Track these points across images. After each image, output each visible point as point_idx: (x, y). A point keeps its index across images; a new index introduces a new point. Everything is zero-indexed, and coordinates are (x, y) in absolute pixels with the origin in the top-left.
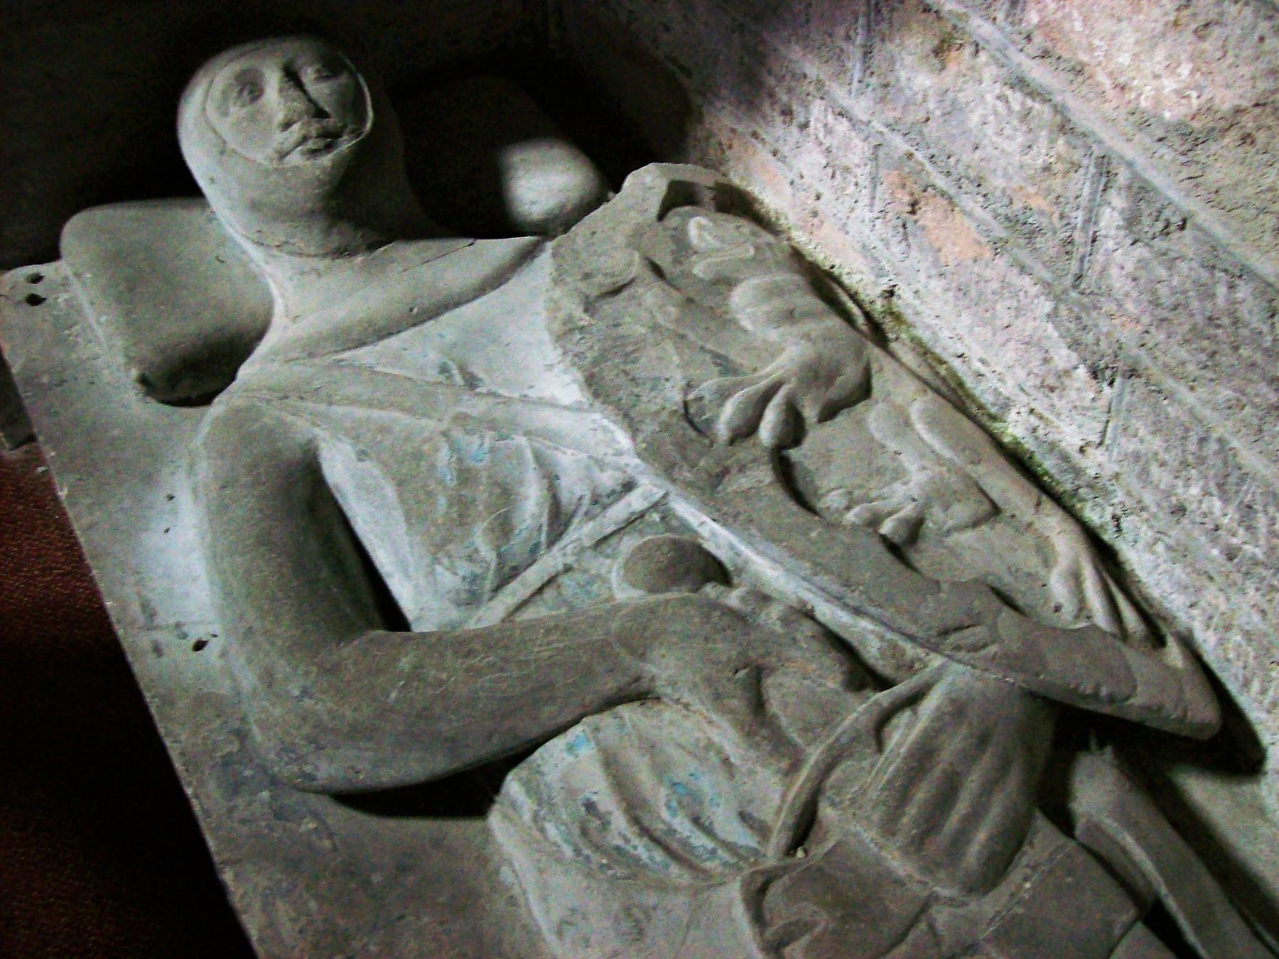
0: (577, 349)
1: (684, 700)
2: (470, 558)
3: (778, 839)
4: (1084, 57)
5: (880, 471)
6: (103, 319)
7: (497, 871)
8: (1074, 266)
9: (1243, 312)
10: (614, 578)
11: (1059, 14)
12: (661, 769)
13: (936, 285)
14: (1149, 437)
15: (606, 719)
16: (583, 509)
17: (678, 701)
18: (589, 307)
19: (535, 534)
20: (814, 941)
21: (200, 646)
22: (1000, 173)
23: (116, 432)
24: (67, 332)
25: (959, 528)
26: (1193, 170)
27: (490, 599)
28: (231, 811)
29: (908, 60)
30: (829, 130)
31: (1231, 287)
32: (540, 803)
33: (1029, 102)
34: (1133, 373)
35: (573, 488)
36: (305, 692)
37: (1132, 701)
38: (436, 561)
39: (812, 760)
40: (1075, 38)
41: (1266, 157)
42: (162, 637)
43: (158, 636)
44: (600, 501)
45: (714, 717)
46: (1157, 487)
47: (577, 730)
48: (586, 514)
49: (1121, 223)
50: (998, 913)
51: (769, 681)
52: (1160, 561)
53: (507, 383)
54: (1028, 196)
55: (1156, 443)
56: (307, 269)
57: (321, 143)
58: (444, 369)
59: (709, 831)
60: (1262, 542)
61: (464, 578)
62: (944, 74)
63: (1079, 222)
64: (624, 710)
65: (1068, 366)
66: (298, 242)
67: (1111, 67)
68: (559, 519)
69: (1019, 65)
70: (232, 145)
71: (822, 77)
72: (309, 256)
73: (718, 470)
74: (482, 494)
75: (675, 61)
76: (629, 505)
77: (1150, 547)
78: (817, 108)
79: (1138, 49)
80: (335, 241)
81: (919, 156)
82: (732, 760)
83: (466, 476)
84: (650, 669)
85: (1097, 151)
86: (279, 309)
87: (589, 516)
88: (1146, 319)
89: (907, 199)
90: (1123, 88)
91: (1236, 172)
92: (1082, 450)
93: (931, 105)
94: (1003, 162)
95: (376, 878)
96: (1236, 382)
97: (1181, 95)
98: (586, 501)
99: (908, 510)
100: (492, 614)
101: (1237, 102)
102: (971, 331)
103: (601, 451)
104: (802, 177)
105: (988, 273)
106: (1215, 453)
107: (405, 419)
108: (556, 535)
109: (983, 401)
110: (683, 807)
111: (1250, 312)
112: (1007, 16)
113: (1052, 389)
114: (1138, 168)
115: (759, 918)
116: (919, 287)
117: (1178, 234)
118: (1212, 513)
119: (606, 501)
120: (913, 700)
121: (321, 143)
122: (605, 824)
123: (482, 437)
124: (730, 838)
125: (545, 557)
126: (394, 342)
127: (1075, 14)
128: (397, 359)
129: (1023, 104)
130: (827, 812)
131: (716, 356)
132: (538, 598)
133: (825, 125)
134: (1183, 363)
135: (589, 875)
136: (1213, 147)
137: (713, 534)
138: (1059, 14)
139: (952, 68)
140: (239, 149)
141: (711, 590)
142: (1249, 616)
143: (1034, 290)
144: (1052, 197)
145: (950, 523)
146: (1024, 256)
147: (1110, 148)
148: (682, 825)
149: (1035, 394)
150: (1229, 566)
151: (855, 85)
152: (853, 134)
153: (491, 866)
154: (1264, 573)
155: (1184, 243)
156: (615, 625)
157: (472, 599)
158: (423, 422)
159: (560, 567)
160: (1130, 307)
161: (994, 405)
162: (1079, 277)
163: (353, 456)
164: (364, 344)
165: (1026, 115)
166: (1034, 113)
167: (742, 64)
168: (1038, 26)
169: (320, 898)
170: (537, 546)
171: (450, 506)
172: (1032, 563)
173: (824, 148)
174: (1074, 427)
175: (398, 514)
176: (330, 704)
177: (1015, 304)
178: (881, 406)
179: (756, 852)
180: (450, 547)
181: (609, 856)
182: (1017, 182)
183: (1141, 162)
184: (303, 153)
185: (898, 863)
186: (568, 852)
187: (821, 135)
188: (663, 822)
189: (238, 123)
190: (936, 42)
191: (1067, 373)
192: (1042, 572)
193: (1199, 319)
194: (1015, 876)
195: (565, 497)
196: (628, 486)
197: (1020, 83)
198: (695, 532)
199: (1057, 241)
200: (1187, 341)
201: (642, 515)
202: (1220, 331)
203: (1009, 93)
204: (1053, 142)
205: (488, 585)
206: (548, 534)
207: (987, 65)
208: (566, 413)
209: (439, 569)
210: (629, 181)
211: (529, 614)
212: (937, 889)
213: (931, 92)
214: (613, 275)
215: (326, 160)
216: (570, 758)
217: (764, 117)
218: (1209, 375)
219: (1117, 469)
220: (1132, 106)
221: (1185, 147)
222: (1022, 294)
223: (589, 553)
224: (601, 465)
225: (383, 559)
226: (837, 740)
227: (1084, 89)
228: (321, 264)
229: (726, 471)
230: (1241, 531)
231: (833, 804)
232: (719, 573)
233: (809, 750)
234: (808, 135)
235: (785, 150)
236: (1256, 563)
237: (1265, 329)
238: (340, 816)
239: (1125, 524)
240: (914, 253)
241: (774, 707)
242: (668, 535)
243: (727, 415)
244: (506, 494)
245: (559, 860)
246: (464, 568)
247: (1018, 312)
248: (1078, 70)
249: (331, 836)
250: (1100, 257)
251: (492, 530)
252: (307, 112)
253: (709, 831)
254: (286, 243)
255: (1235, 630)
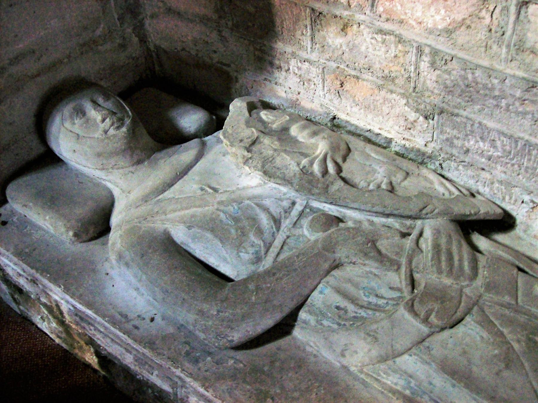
0: (253, 165)
1: (353, 261)
2: (252, 246)
3: (406, 291)
4: (403, 17)
5: (368, 173)
6: (47, 218)
7: (304, 349)
8: (412, 85)
9: (479, 80)
10: (306, 232)
11: (391, 6)
12: (356, 286)
13: (356, 109)
14: (452, 132)
15: (328, 278)
16: (283, 216)
17: (351, 262)
18: (249, 150)
19: (271, 230)
20: (437, 312)
21: (152, 320)
22: (377, 63)
23: (69, 259)
24: (25, 230)
25: (401, 181)
26: (452, 41)
27: (265, 257)
28: (199, 369)
29: (331, 35)
30: (299, 69)
31: (473, 74)
32: (317, 315)
33: (384, 37)
34: (441, 112)
35: (275, 210)
36: (218, 311)
37: (481, 212)
38: (239, 251)
39: (404, 263)
40: (399, 12)
41: (476, 31)
42: (136, 323)
43: (132, 323)
44: (288, 211)
45: (367, 262)
46: (458, 147)
47: (321, 286)
48: (285, 217)
49: (429, 65)
50: (482, 283)
51: (377, 244)
52: (461, 172)
53: (228, 186)
54: (390, 67)
55: (455, 132)
56: (127, 173)
57: (119, 124)
58: (202, 189)
59: (382, 297)
60: (500, 150)
61: (253, 253)
62: (347, 36)
63: (413, 70)
64: (333, 273)
65: (415, 119)
66: (121, 163)
67: (415, 17)
68: (277, 222)
69: (379, 25)
70: (81, 134)
71: (294, 51)
72: (126, 167)
73: (325, 186)
74: (245, 223)
75: (222, 63)
76: (297, 209)
77: (457, 169)
78: (293, 62)
79: (423, 10)
80: (135, 159)
81: (342, 66)
82: (377, 273)
83: (236, 220)
84: (337, 255)
85: (415, 45)
86: (116, 192)
87: (286, 218)
88: (443, 94)
89: (339, 83)
90: (420, 23)
91: (467, 38)
92: (426, 145)
93: (344, 48)
94: (378, 59)
95: (266, 369)
96: (480, 102)
97: (443, 19)
98: (283, 213)
99: (385, 180)
100: (268, 263)
101: (463, 17)
102: (373, 120)
103: (278, 196)
104: (290, 88)
105: (378, 98)
106: (478, 128)
107: (200, 210)
108: (278, 229)
109: (380, 143)
110: (371, 294)
111: (481, 79)
112: (371, 11)
113: (410, 129)
114: (433, 46)
115: (416, 314)
116: (348, 112)
117: (450, 63)
118: (480, 147)
119: (289, 210)
120: (421, 234)
121: (119, 124)
122: (346, 311)
123: (232, 206)
124: (391, 297)
125: (278, 236)
126: (177, 186)
127: (397, 4)
128: (181, 192)
129: (382, 38)
130: (416, 276)
131: (299, 153)
132: (282, 250)
133: (298, 67)
134: (460, 103)
135: (347, 330)
136: (457, 33)
137: (329, 209)
138: (391, 6)
139: (350, 34)
140: (86, 135)
141: (341, 225)
142: (500, 175)
143: (397, 98)
144: (400, 65)
145: (399, 181)
146: (392, 87)
147: (421, 43)
148: (373, 300)
149: (404, 132)
150: (490, 162)
151: (309, 49)
152: (311, 67)
153: (302, 348)
154: (503, 159)
155: (454, 65)
156: (320, 246)
157: (258, 259)
158: (207, 208)
159: (285, 237)
160: (436, 91)
161: (384, 143)
162: (415, 88)
163: (187, 229)
164: (165, 191)
165: (384, 41)
166: (387, 39)
167: (255, 55)
168: (383, 12)
169: (248, 384)
170: (274, 233)
171: (237, 231)
172: (428, 185)
173: (298, 76)
174: (421, 139)
175: (217, 242)
176: (231, 311)
177: (390, 104)
178: (356, 153)
179: (400, 297)
180: (243, 244)
181: (352, 321)
182: (385, 63)
183: (433, 44)
184: (114, 129)
185: (448, 281)
186: (335, 326)
187: (296, 72)
188: (366, 301)
189: (81, 126)
190: (342, 27)
191: (415, 121)
192: (432, 186)
193: (463, 87)
194: (480, 271)
195: (275, 214)
196: (294, 203)
197: (381, 31)
198: (323, 211)
199: (404, 79)
200: (460, 95)
201: (303, 211)
202: (471, 89)
203: (376, 36)
204: (396, 47)
205: (263, 252)
206: (276, 228)
207: (364, 29)
208: (257, 188)
209: (241, 254)
210: (231, 107)
211: (282, 257)
212: (463, 284)
213: (343, 43)
214: (249, 138)
215: (124, 129)
216: (322, 296)
217: (268, 72)
218: (471, 103)
219: (440, 146)
220: (426, 27)
221: (447, 36)
222: (393, 101)
223: (293, 229)
224: (281, 200)
225: (212, 261)
226: (408, 253)
227: (405, 27)
228: (131, 169)
229: (328, 186)
230: (492, 149)
231: (418, 273)
232: (339, 220)
233: (401, 260)
234: (290, 73)
235: (281, 81)
236: (499, 157)
237: (488, 82)
238: (240, 355)
239: (443, 165)
240: (344, 101)
241: (384, 251)
242: (315, 215)
243: (316, 168)
244: (254, 220)
245: (333, 331)
246: (251, 250)
247: (392, 107)
248: (401, 22)
249: (241, 362)
250: (422, 79)
251: (256, 233)
252: (109, 114)
253: (382, 297)
254: (116, 165)
255: (496, 182)
